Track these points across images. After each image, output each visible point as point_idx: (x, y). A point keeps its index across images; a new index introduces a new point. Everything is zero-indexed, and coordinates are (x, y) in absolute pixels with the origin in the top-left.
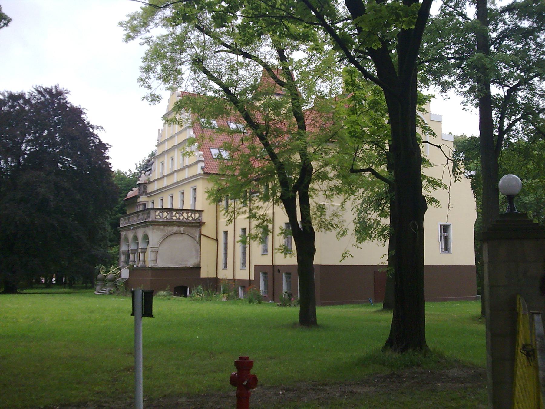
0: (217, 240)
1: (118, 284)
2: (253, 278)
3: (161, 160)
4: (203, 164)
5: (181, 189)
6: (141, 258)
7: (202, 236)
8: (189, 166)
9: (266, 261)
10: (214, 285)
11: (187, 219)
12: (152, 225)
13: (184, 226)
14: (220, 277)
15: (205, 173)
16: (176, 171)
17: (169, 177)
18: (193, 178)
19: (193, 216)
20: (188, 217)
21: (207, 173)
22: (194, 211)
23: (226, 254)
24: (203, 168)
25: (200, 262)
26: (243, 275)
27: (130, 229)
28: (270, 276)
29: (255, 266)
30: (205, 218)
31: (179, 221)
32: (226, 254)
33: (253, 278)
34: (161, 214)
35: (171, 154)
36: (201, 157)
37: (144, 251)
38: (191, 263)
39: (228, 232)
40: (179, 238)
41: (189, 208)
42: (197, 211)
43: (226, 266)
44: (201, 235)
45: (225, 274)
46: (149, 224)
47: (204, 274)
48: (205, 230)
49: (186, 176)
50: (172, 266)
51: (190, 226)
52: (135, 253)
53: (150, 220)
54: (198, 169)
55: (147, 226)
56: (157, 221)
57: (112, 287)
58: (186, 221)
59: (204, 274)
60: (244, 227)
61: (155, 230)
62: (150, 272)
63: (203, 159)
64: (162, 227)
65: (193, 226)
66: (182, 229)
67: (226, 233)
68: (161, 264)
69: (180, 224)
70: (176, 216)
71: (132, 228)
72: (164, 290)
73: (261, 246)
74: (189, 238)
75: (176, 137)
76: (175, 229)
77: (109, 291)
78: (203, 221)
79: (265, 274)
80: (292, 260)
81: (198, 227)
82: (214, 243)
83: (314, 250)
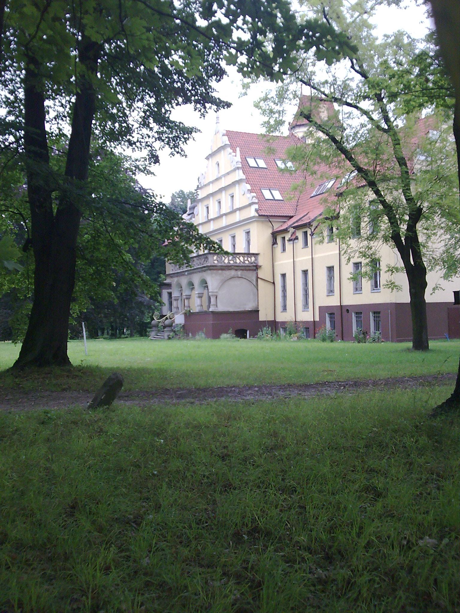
0: (274, 283)
1: (176, 329)
2: (317, 319)
3: (205, 203)
4: (256, 206)
5: (232, 232)
6: (186, 304)
7: (259, 280)
8: (240, 209)
9: (333, 301)
10: (274, 326)
11: (244, 263)
12: (210, 270)
13: (241, 270)
14: (278, 320)
15: (260, 216)
16: (225, 214)
17: (216, 221)
18: (248, 221)
19: (249, 259)
20: (244, 260)
21: (262, 215)
22: (249, 254)
23: (284, 297)
24: (256, 211)
25: (258, 305)
26: (307, 316)
27: (184, 275)
28: (337, 317)
29: (319, 307)
30: (261, 261)
31: (236, 265)
32: (284, 297)
33: (317, 319)
34: (219, 259)
35: (218, 197)
36: (254, 198)
37: (189, 298)
38: (249, 307)
39: (287, 275)
40: (237, 282)
41: (243, 252)
42: (253, 254)
43: (285, 308)
44: (258, 278)
45: (281, 317)
46: (207, 270)
47: (262, 317)
48: (261, 274)
49: (237, 220)
50: (231, 310)
51: (246, 270)
52: (178, 300)
53: (209, 265)
54: (252, 212)
55: (205, 271)
56: (216, 266)
57: (171, 332)
58: (243, 265)
59: (262, 317)
60: (330, 265)
61: (214, 275)
62: (211, 315)
63: (257, 201)
64: (220, 271)
65: (250, 270)
66: (239, 273)
67: (284, 276)
68: (221, 308)
69: (237, 268)
70: (239, 260)
71: (186, 273)
72: (226, 332)
73: (369, 282)
74: (246, 280)
75: (223, 178)
76: (233, 273)
77: (168, 336)
78: (260, 264)
79: (332, 315)
80: (405, 297)
81: (255, 270)
82: (271, 286)
83: (426, 284)
